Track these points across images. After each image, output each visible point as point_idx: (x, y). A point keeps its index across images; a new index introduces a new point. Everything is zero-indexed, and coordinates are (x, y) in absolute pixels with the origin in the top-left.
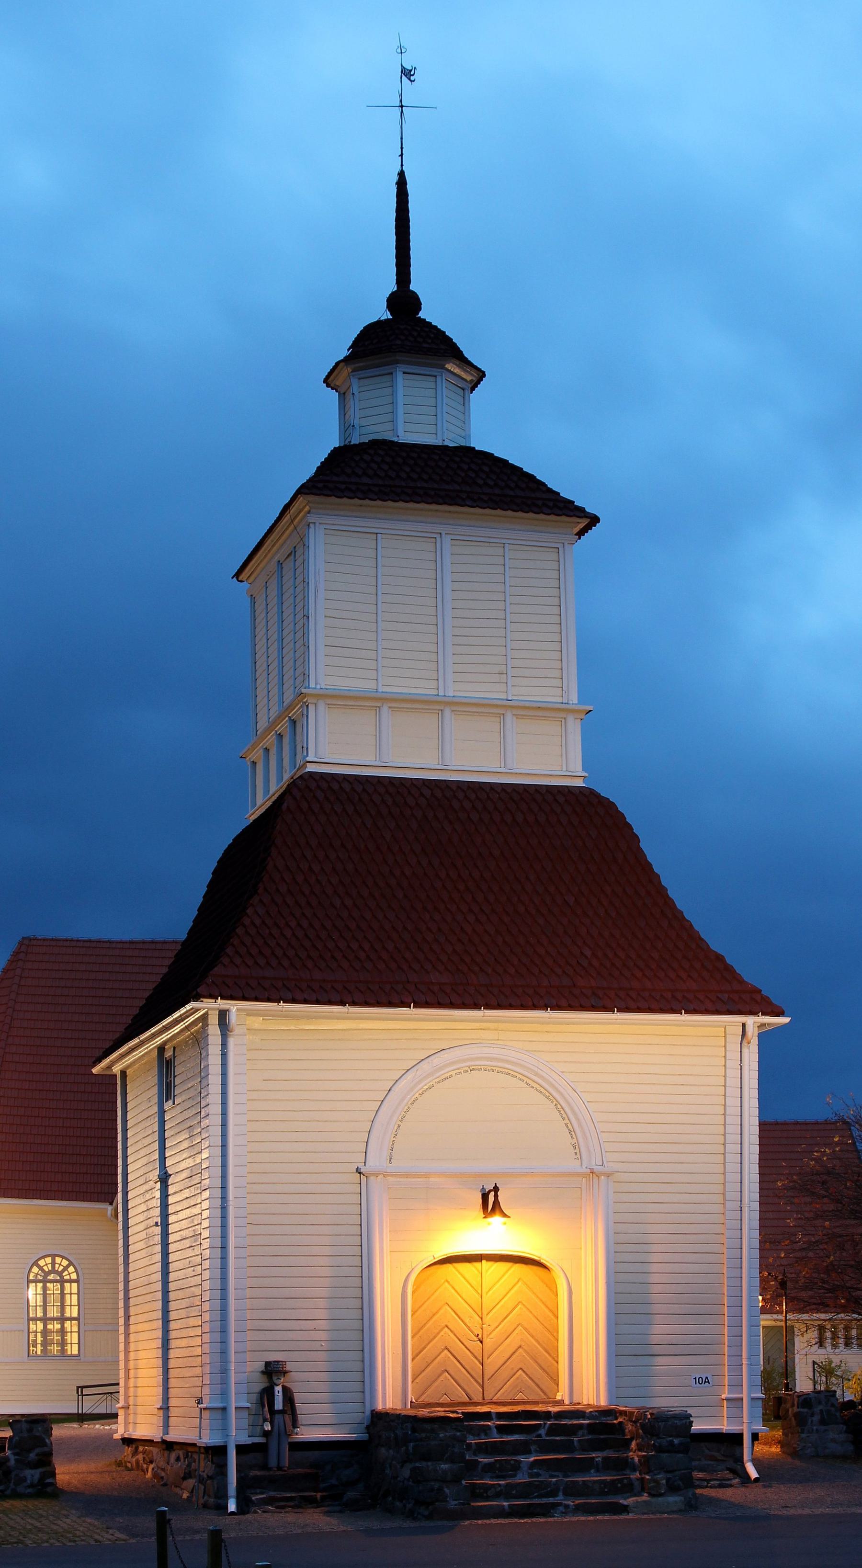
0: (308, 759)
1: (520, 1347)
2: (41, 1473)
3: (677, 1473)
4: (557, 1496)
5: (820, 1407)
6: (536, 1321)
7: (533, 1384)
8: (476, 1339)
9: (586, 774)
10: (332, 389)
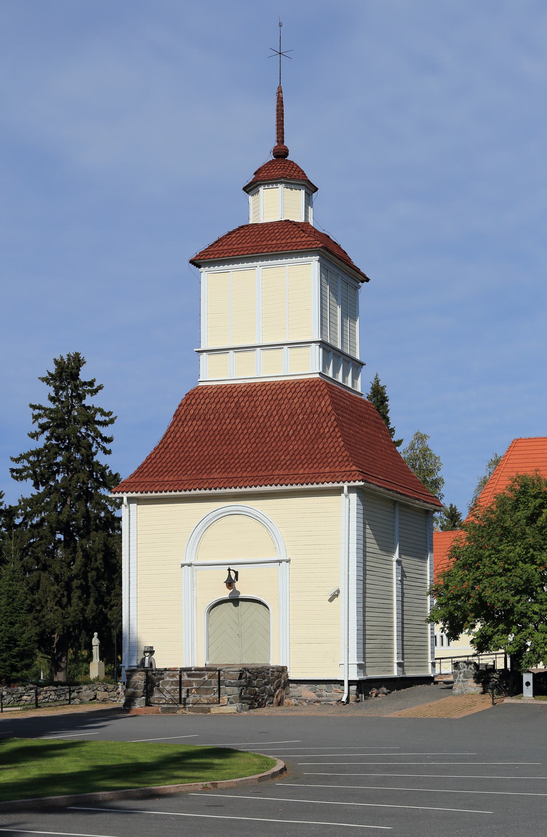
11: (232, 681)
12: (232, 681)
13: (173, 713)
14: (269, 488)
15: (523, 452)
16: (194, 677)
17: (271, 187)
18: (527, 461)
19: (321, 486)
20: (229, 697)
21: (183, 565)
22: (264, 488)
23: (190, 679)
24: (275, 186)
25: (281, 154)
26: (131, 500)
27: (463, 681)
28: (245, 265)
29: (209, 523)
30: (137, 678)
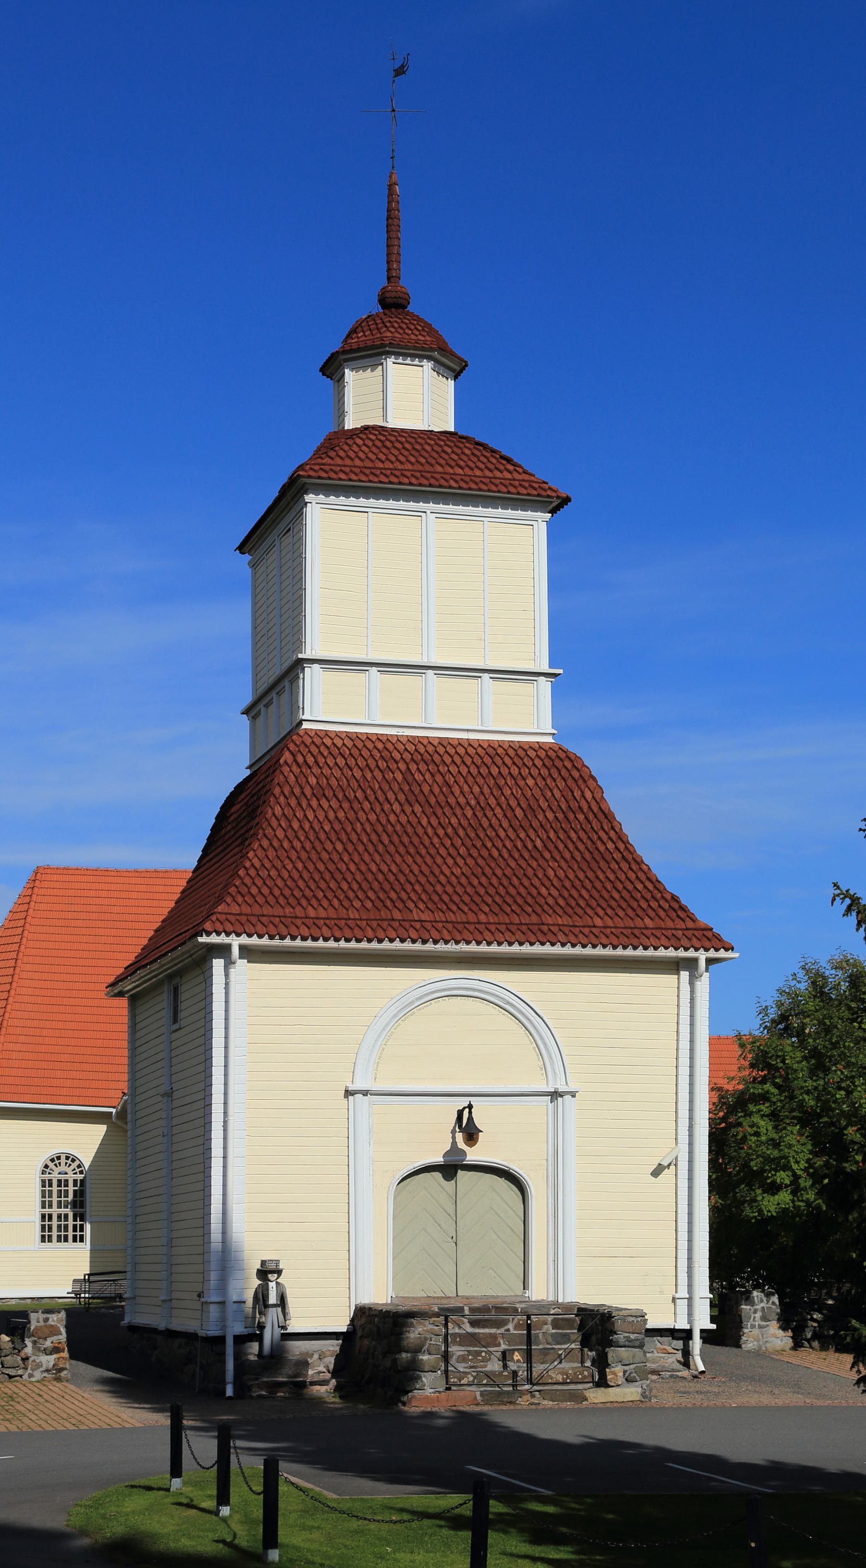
0: (304, 718)
3: (632, 1366)
4: (765, 1084)
5: (762, 1305)
9: (555, 732)
10: (328, 377)
11: (632, 1336)
12: (632, 1336)
13: (511, 1403)
14: (547, 949)
15: (60, 892)
16: (484, 1327)
17: (408, 361)
18: (72, 908)
19: (650, 952)
20: (626, 1368)
21: (348, 1093)
22: (537, 949)
23: (477, 1330)
24: (416, 362)
25: (393, 303)
26: (247, 952)
27: (760, 1327)
28: (402, 504)
29: (409, 1008)
30: (427, 1331)
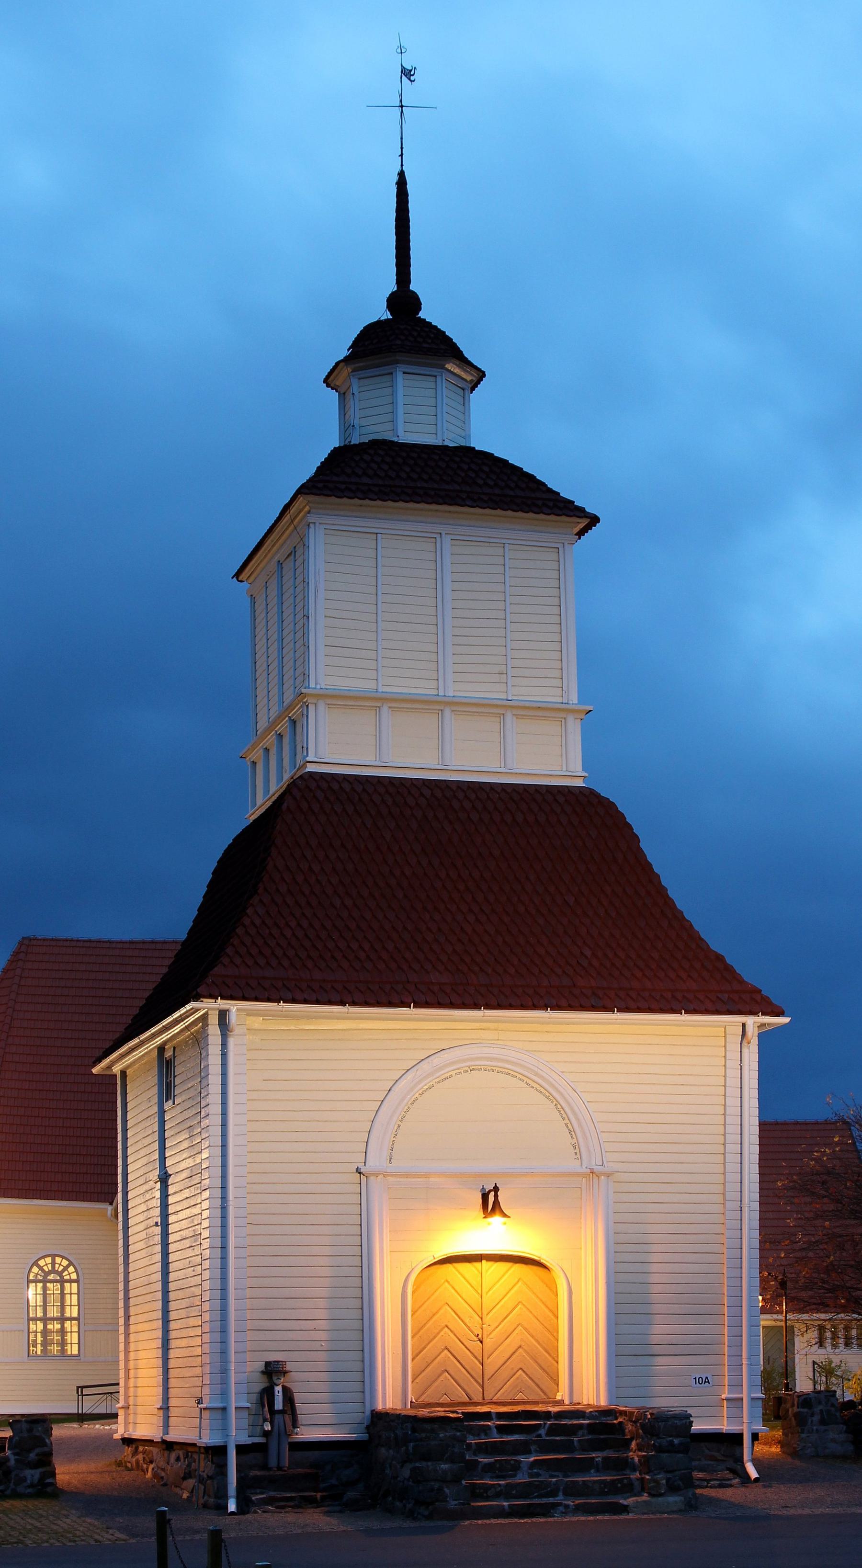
0: (308, 759)
1: (520, 1347)
2: (41, 1473)
3: (677, 1473)
5: (820, 1407)
6: (536, 1321)
7: (533, 1384)
8: (476, 1339)
9: (586, 774)
10: (332, 389)
